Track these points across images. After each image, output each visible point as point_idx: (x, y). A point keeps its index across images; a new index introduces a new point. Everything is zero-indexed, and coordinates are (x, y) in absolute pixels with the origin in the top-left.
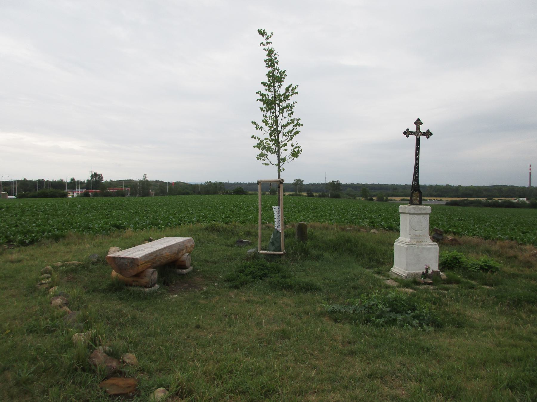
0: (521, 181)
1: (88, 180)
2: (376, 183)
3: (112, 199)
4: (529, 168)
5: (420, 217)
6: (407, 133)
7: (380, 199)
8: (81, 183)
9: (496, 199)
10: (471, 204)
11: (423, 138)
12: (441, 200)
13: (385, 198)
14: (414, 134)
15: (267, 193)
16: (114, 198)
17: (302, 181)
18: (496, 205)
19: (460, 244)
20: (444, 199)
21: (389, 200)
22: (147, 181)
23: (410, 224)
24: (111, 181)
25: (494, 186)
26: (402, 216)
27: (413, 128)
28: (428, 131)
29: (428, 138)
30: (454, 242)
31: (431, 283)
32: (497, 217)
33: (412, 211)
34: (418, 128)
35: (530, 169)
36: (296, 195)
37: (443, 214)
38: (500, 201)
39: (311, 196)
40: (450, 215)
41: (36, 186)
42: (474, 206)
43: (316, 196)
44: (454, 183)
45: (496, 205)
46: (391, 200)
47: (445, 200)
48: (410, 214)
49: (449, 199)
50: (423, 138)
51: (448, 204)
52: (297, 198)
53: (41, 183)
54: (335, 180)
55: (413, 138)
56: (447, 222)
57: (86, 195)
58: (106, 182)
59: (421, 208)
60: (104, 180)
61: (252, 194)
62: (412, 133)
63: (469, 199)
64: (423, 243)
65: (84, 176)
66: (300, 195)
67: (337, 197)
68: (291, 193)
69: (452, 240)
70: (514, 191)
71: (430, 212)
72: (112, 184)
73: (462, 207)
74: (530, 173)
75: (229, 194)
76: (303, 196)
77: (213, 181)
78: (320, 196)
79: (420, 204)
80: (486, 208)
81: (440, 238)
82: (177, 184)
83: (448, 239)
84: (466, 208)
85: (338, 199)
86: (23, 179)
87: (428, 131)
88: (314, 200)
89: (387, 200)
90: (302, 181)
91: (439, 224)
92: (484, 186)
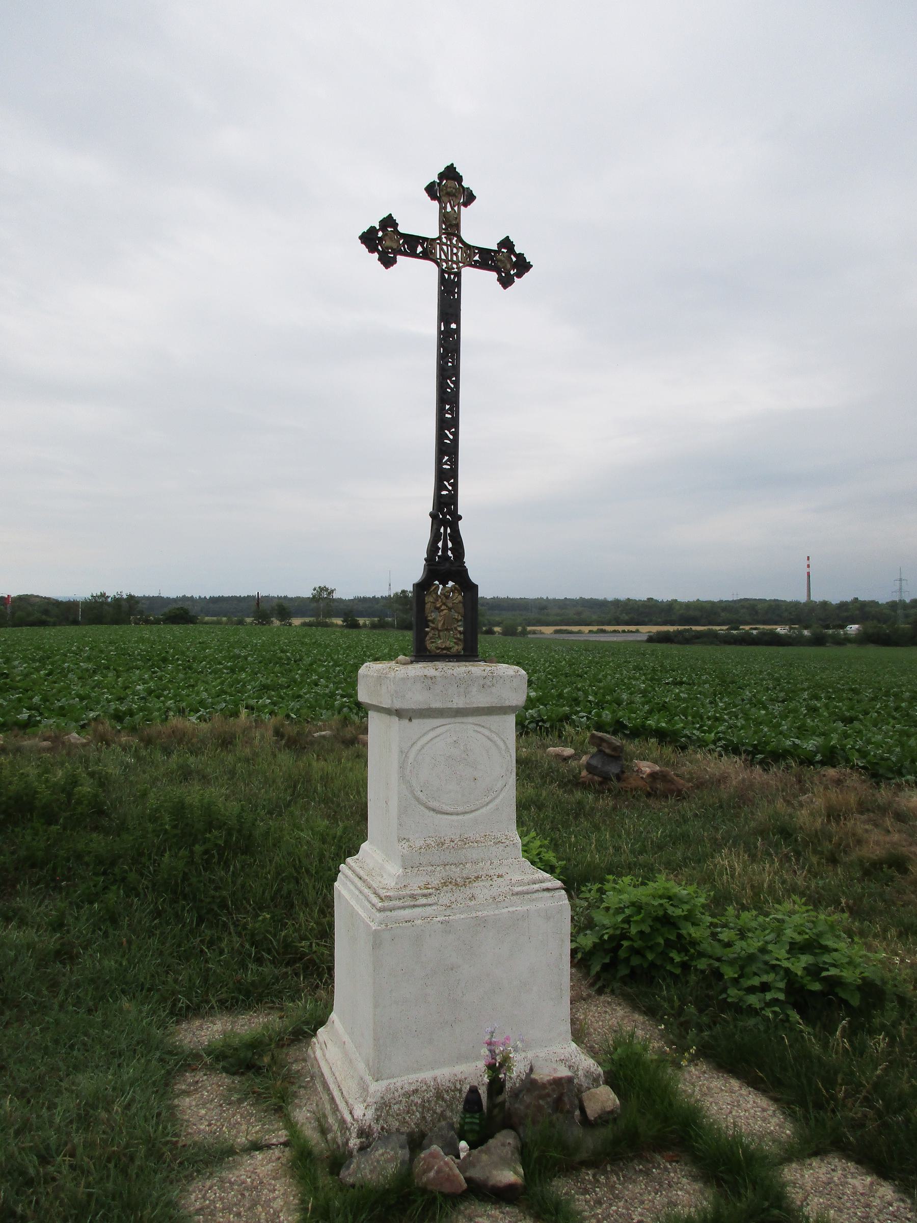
0: (791, 592)
2: (502, 595)
4: (807, 563)
5: (468, 728)
6: (386, 241)
7: (509, 632)
9: (747, 628)
10: (697, 638)
11: (477, 283)
12: (637, 631)
13: (520, 629)
14: (427, 255)
15: (249, 620)
17: (332, 591)
18: (747, 640)
19: (680, 795)
20: (644, 629)
21: (530, 632)
23: (402, 777)
25: (741, 600)
26: (376, 723)
27: (422, 219)
28: (507, 243)
29: (506, 282)
30: (660, 786)
31: (511, 1187)
32: (761, 672)
33: (416, 698)
34: (450, 225)
35: (808, 566)
36: (318, 624)
37: (637, 668)
38: (755, 632)
39: (354, 625)
40: (654, 670)
42: (704, 643)
43: (365, 625)
44: (663, 595)
45: (747, 640)
46: (534, 632)
47: (647, 630)
48: (399, 713)
49: (655, 629)
50: (477, 283)
51: (651, 640)
52: (318, 632)
55: (419, 277)
56: (644, 693)
61: (212, 623)
62: (413, 246)
63: (694, 628)
64: (482, 891)
66: (326, 625)
68: (307, 620)
69: (653, 776)
70: (775, 611)
73: (679, 646)
74: (808, 574)
75: (153, 623)
77: (111, 593)
78: (374, 626)
79: (469, 654)
80: (729, 649)
81: (613, 769)
82: (23, 600)
83: (639, 771)
84: (689, 650)
87: (507, 243)
88: (363, 635)
89: (524, 633)
90: (332, 591)
91: (619, 702)
92: (721, 601)
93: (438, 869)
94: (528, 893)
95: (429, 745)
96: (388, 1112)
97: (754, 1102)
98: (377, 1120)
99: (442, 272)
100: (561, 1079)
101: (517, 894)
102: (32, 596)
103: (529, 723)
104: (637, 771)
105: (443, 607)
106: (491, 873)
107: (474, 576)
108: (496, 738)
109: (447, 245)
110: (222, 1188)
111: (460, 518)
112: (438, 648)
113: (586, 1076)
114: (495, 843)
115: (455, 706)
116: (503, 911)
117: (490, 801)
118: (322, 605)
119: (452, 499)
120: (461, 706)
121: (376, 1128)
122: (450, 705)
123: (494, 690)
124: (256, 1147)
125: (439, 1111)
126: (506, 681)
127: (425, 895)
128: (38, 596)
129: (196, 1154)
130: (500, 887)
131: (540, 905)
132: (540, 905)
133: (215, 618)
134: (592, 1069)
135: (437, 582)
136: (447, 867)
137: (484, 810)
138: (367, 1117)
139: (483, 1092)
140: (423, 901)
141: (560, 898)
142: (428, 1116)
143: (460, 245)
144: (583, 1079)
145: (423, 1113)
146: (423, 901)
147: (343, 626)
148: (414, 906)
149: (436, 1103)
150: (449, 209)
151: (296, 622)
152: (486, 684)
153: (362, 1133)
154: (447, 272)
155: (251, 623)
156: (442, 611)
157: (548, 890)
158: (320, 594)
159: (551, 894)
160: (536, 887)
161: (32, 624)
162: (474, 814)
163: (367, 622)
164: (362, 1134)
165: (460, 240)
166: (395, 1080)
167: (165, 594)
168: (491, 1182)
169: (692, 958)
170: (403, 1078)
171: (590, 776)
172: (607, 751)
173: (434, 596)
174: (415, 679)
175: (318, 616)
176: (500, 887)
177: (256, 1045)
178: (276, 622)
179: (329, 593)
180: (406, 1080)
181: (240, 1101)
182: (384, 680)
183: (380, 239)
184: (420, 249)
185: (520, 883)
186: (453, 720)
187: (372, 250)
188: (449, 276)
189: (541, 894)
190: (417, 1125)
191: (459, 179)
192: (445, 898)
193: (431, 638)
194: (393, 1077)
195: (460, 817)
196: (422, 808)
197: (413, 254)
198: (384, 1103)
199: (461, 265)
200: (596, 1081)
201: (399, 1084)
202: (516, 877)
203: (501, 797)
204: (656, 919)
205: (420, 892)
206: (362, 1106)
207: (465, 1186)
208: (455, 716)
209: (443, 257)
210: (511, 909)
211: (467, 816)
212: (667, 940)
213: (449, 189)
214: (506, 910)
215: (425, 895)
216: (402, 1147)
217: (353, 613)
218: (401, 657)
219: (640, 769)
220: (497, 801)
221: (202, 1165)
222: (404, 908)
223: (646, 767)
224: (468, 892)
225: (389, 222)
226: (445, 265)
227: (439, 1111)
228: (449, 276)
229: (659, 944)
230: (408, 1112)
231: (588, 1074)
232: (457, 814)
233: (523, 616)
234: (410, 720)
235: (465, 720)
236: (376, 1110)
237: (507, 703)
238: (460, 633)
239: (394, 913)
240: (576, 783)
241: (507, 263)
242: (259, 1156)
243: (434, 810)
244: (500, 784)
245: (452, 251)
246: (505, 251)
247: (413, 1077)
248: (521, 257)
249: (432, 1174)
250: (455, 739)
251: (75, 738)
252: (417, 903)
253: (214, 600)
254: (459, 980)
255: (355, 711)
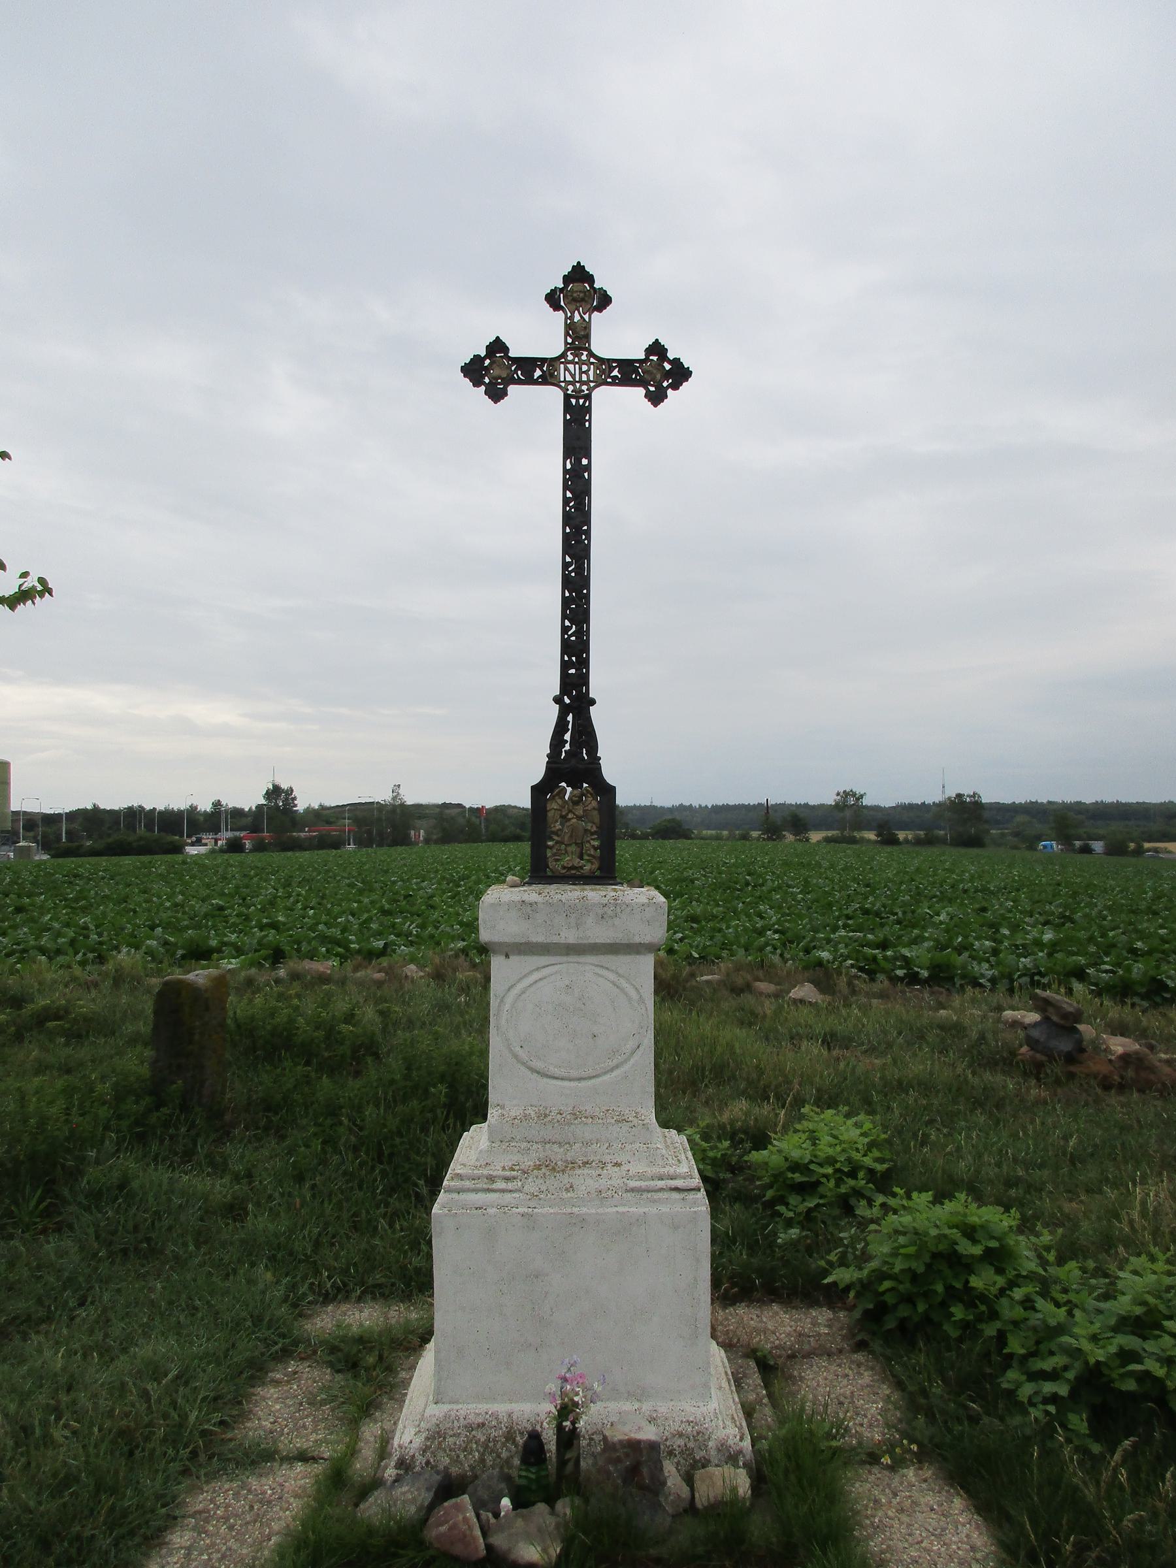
1: (259, 807)
2: (1109, 798)
3: (304, 856)
8: (237, 813)
11: (616, 409)
13: (1132, 845)
15: (755, 834)
16: (307, 854)
17: (862, 796)
22: (403, 805)
24: (323, 808)
27: (539, 334)
28: (657, 349)
29: (656, 398)
34: (578, 337)
39: (889, 840)
41: (118, 823)
43: (907, 841)
50: (616, 409)
53: (133, 815)
54: (967, 791)
55: (541, 406)
57: (235, 846)
58: (309, 811)
59: (577, 913)
60: (301, 806)
61: (711, 838)
62: (532, 370)
64: (585, 1180)
65: (249, 798)
66: (853, 841)
67: (974, 842)
68: (830, 833)
71: (657, 933)
72: (322, 816)
76: (863, 841)
78: (918, 842)
83: (1107, 1050)
85: (974, 851)
86: (89, 807)
87: (657, 349)
90: (862, 796)
93: (535, 1146)
94: (648, 1191)
95: (532, 989)
96: (440, 1443)
97: (967, 1536)
98: (424, 1451)
99: (567, 398)
100: (639, 1442)
101: (632, 1190)
102: (509, 806)
103: (1020, 977)
104: (1105, 1050)
105: (570, 816)
106: (607, 1158)
107: (610, 773)
108: (623, 983)
109: (576, 362)
110: (236, 1495)
111: (593, 702)
112: (564, 867)
113: (719, 1450)
114: (618, 1121)
115: (563, 941)
116: (610, 1210)
117: (617, 1067)
118: (848, 813)
119: (583, 680)
120: (571, 940)
121: (420, 1460)
122: (556, 939)
123: (617, 921)
124: (304, 1457)
125: (504, 1455)
126: (639, 909)
127: (507, 1179)
128: (515, 807)
129: (231, 1451)
130: (613, 1177)
131: (665, 1209)
132: (665, 1209)
133: (714, 832)
134: (730, 1442)
135: (563, 784)
136: (548, 1146)
137: (606, 1078)
138: (413, 1445)
139: (549, 1436)
140: (501, 1185)
141: (695, 1203)
142: (489, 1459)
143: (592, 360)
144: (713, 1453)
145: (482, 1455)
146: (501, 1185)
147: (876, 842)
148: (489, 1190)
149: (504, 1445)
150: (577, 318)
151: (815, 836)
152: (577, 913)
153: (402, 1464)
154: (573, 397)
155: (758, 839)
156: (573, 817)
157: (677, 1189)
158: (845, 801)
159: (682, 1195)
160: (661, 1184)
161: (506, 840)
162: (593, 1081)
163: (910, 837)
164: (402, 1464)
165: (591, 354)
166: (455, 1407)
167: (658, 803)
168: (513, 1556)
169: (980, 1319)
170: (470, 1406)
171: (1031, 1053)
172: (1055, 1018)
173: (560, 801)
174: (510, 905)
175: (843, 829)
176: (613, 1177)
177: (363, 1341)
178: (790, 837)
179: (858, 799)
180: (472, 1410)
181: (323, 1403)
182: (505, 909)
183: (487, 369)
184: (538, 373)
185: (641, 1177)
186: (565, 959)
187: (477, 383)
188: (577, 402)
189: (665, 1195)
190: (472, 1468)
191: (590, 279)
192: (531, 1186)
193: (554, 855)
194: (457, 1402)
195: (573, 1084)
196: (523, 1068)
197: (530, 381)
198: (438, 1433)
199: (592, 385)
200: (732, 1458)
201: (462, 1413)
202: (635, 1168)
203: (632, 1061)
204: (935, 1256)
205: (501, 1173)
206: (413, 1431)
207: (482, 1552)
208: (567, 954)
209: (569, 378)
210: (621, 1209)
211: (583, 1084)
212: (949, 1288)
213: (579, 293)
214: (615, 1209)
215: (507, 1179)
216: (428, 1489)
217: (457, 826)
218: (510, 878)
219: (1108, 1047)
220: (626, 1067)
221: (232, 1465)
222: (476, 1191)
223: (1119, 1045)
224: (566, 1179)
225: (497, 347)
226: (571, 388)
227: (504, 1455)
228: (577, 402)
229: (935, 1292)
230: (465, 1450)
231: (722, 1447)
232: (570, 1080)
233: (671, 826)
234: (507, 956)
235: (582, 959)
236: (427, 1439)
237: (637, 940)
238: (595, 849)
239: (463, 1196)
240: (1006, 1061)
241: (658, 374)
242: (299, 1467)
243: (538, 1073)
244: (631, 1044)
245: (580, 369)
246: (655, 358)
247: (482, 1407)
248: (677, 362)
249: (443, 1529)
250: (567, 982)
251: (411, 971)
252: (494, 1186)
253: (717, 809)
254: (547, 1293)
255: (779, 951)
